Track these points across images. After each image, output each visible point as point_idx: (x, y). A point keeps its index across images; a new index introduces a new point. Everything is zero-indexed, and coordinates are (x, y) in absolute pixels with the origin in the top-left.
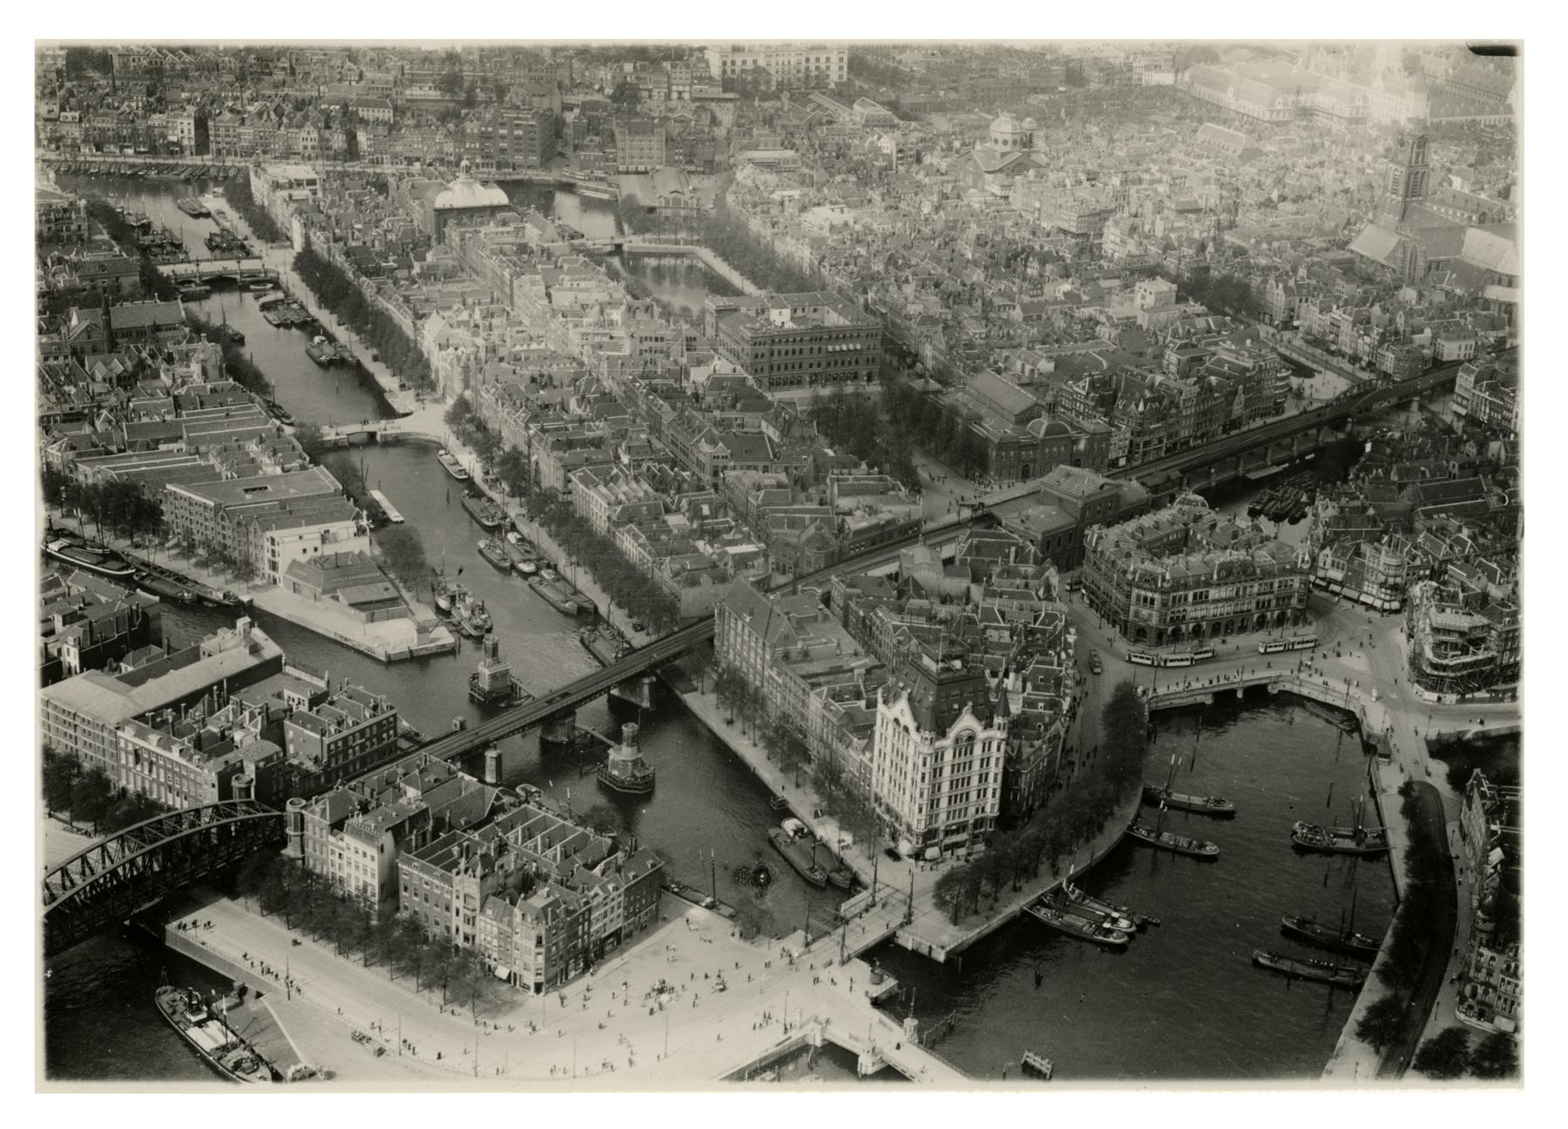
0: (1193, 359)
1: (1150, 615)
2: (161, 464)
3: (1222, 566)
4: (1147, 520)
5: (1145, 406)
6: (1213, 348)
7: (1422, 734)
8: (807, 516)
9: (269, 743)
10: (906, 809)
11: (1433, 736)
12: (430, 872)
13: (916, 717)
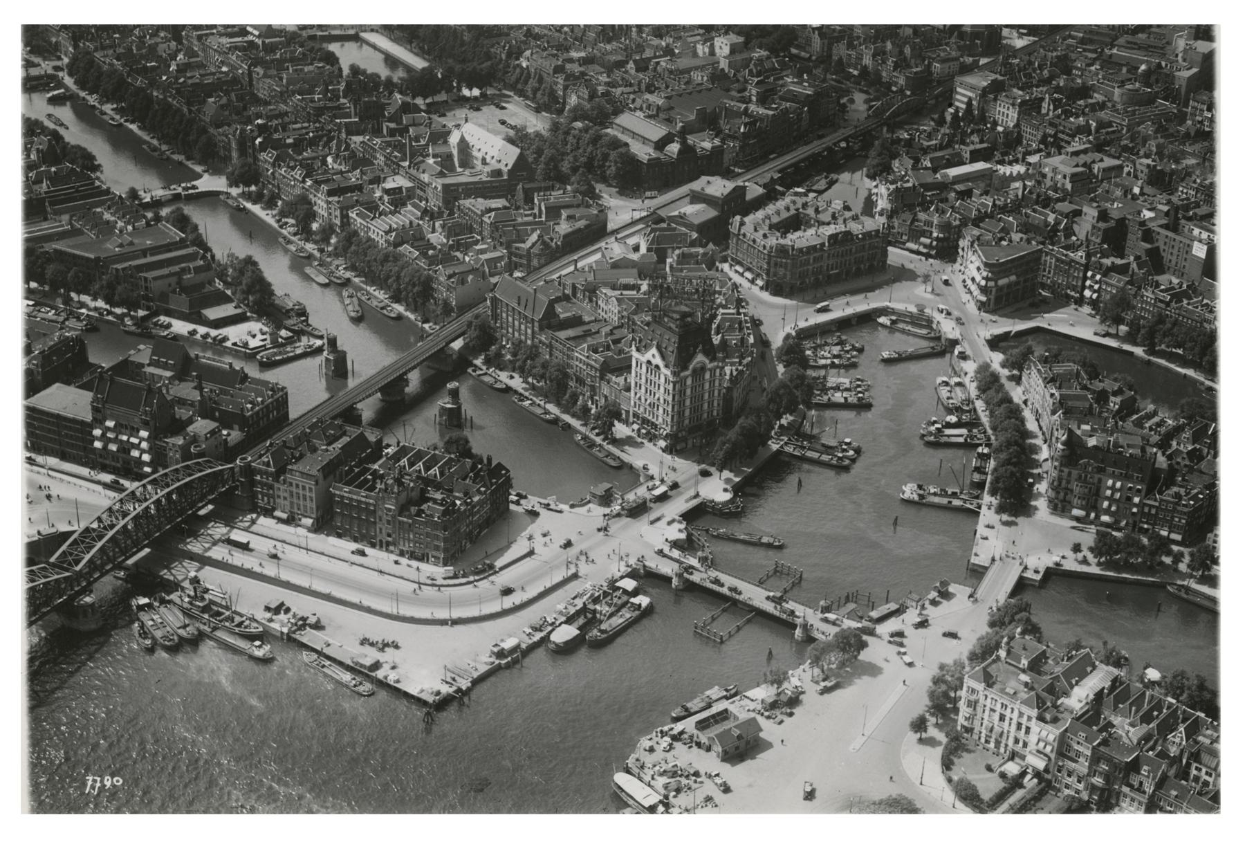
0: (766, 91)
1: (785, 274)
2: (38, 231)
3: (831, 237)
4: (770, 209)
5: (745, 128)
6: (781, 82)
7: (982, 337)
8: (529, 228)
9: (207, 421)
10: (660, 420)
11: (988, 337)
12: (358, 494)
13: (663, 357)
